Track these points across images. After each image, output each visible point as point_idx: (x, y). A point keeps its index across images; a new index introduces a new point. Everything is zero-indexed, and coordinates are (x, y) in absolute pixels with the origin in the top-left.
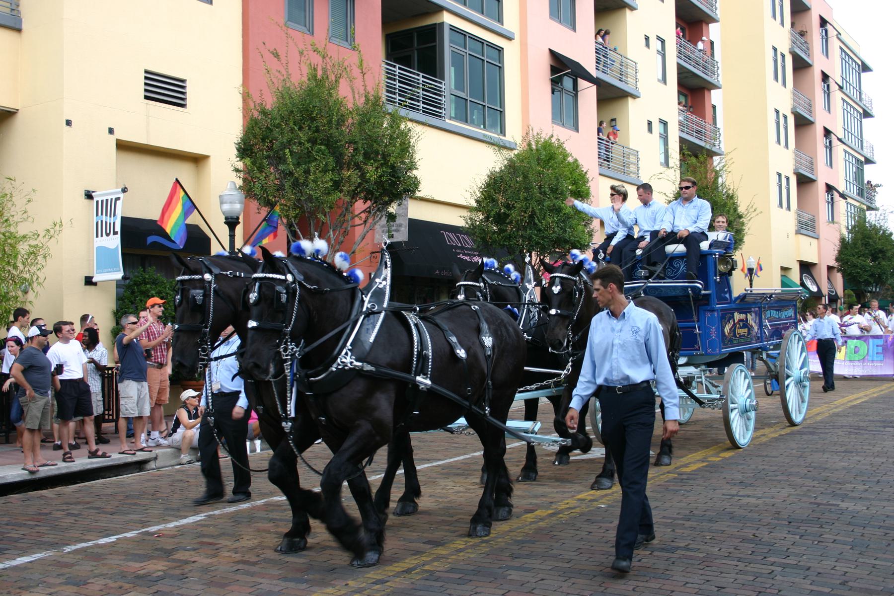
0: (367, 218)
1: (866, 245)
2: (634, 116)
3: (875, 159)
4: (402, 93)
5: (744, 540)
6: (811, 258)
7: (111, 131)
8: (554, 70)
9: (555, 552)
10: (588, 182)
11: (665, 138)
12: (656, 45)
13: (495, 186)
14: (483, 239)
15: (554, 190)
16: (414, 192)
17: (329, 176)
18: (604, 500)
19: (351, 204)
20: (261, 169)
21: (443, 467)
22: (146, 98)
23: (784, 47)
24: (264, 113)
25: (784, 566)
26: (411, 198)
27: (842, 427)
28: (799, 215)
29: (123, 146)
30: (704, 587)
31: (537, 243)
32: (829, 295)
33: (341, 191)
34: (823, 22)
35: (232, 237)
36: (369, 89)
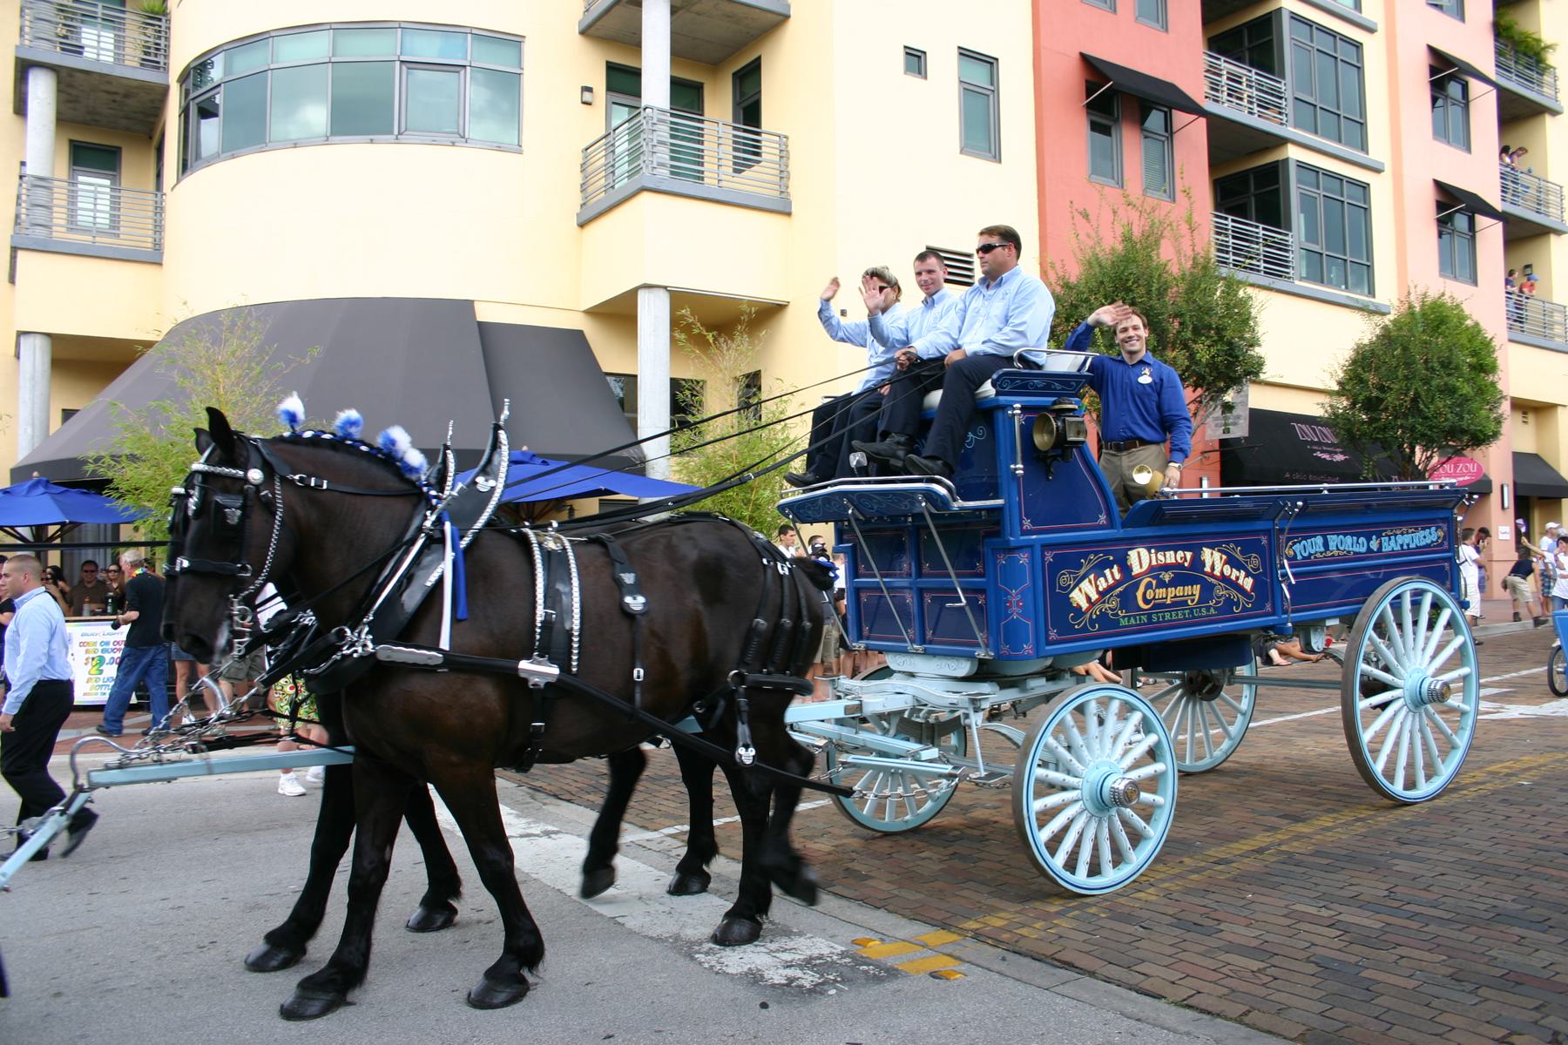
4: (1237, 251)
8: (1440, 206)
9: (1458, 839)
13: (1363, 361)
14: (1349, 431)
15: (1446, 365)
16: (1257, 374)
18: (1526, 775)
31: (1423, 435)
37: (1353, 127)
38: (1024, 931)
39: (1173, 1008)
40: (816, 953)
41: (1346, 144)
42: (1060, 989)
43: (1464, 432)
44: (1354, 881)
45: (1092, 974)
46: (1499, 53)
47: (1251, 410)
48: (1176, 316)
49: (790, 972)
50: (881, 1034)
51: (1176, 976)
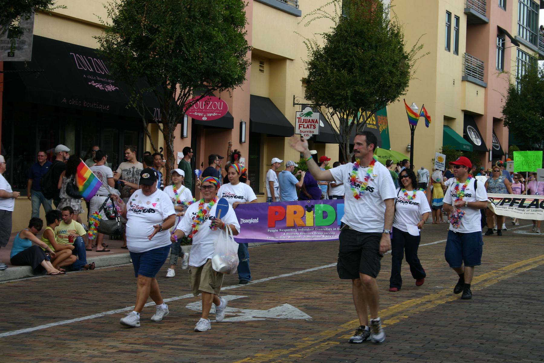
6: (477, 108)
10: (243, 7)
15: (205, 15)
16: (45, 5)
21: (72, 326)
27: (513, 295)
28: (467, 60)
31: (184, 75)
32: (493, 150)
43: (216, 74)
47: (34, 36)
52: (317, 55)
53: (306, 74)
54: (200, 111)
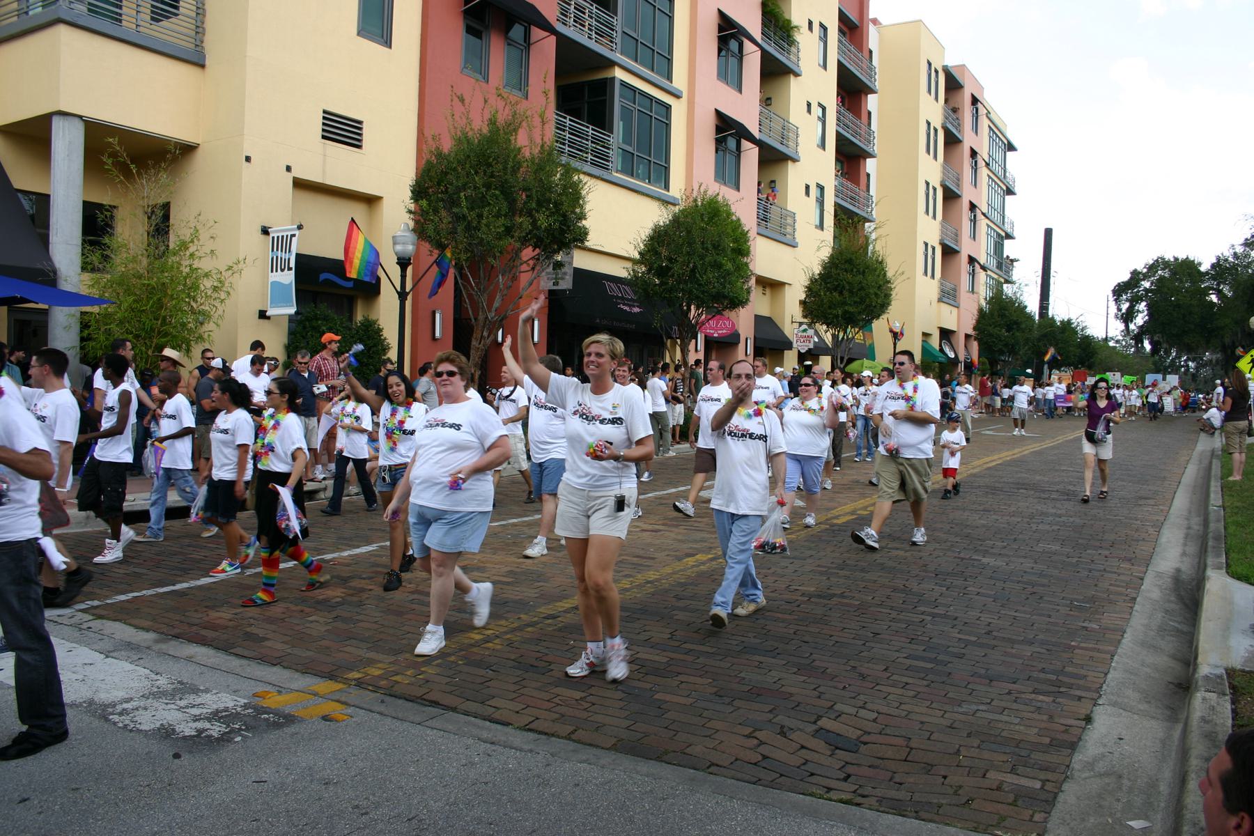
0: (535, 265)
1: (1002, 316)
2: (795, 178)
3: (1015, 234)
4: (572, 144)
5: (895, 590)
6: (951, 326)
7: (289, 169)
8: (719, 130)
11: (821, 202)
12: (817, 111)
13: (658, 238)
14: (645, 290)
15: (716, 247)
16: (582, 241)
17: (502, 221)
19: (520, 250)
20: (436, 211)
22: (324, 137)
23: (937, 122)
24: (439, 155)
25: (934, 616)
26: (579, 248)
29: (299, 184)
30: (860, 632)
31: (697, 297)
33: (512, 237)
34: (975, 101)
35: (403, 277)
36: (546, 139)
37: (662, 61)
38: (397, 678)
39: (518, 732)
40: (222, 706)
41: (657, 73)
42: (429, 723)
43: (725, 297)
44: (647, 628)
45: (454, 709)
46: (764, 24)
47: (575, 269)
48: (524, 190)
49: (200, 725)
50: (283, 772)
51: (520, 707)
52: (813, 281)
53: (803, 297)
54: (711, 328)
